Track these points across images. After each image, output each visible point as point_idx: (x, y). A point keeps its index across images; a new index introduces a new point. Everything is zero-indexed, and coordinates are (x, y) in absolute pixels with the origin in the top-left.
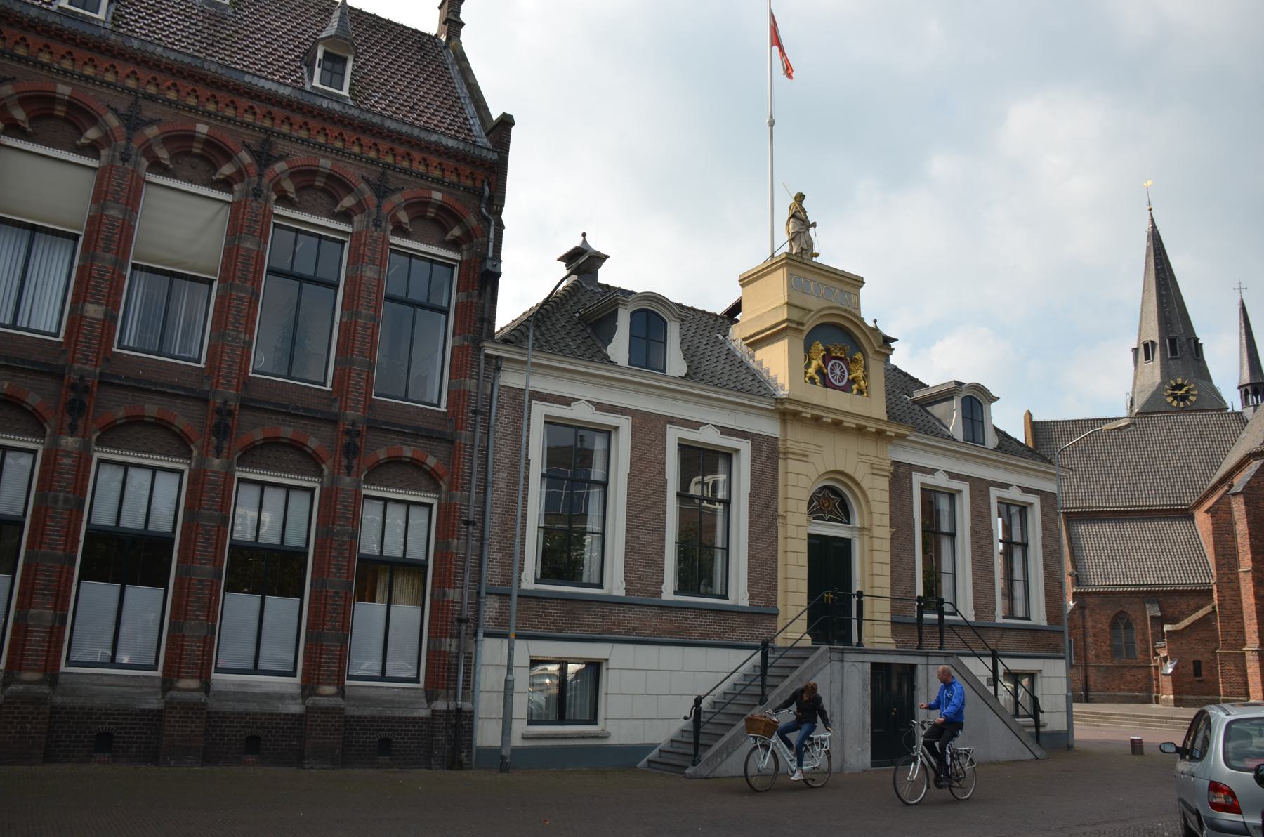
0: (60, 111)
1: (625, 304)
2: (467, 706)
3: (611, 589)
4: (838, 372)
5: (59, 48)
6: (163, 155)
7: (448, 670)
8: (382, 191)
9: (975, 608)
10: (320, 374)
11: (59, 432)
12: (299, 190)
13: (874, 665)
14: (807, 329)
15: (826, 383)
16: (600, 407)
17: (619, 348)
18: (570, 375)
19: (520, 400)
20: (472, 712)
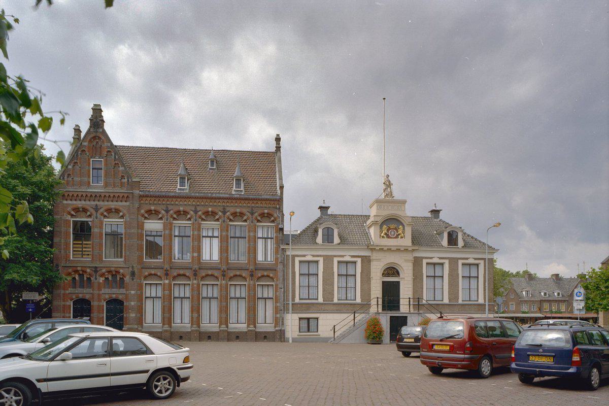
0: (266, 215)
2: (283, 329)
5: (179, 200)
6: (203, 217)
7: (279, 321)
8: (252, 214)
10: (243, 260)
11: (164, 280)
12: (234, 217)
14: (380, 223)
15: (388, 237)
16: (313, 256)
17: (319, 239)
20: (284, 330)
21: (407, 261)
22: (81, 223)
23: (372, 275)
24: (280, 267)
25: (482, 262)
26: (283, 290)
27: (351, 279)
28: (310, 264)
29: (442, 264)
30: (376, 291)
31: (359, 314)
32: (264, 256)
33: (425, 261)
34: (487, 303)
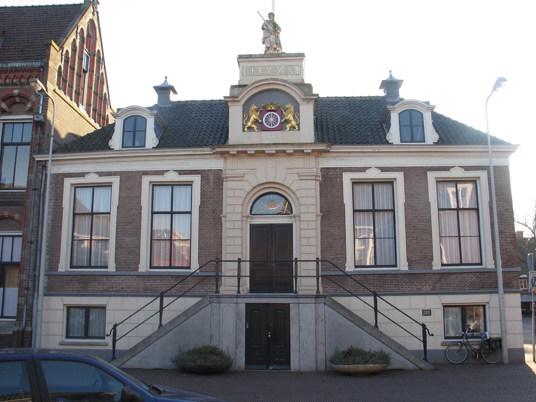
1: (394, 109)
2: (28, 329)
3: (486, 265)
4: (271, 120)
9: (408, 260)
13: (247, 304)
17: (394, 134)
18: (444, 154)
19: (59, 179)
21: (302, 177)
23: (227, 209)
24: (32, 199)
25: (483, 175)
26: (33, 246)
27: (383, 219)
28: (375, 186)
29: (391, 183)
30: (236, 246)
31: (172, 299)
33: (347, 178)
34: (500, 270)
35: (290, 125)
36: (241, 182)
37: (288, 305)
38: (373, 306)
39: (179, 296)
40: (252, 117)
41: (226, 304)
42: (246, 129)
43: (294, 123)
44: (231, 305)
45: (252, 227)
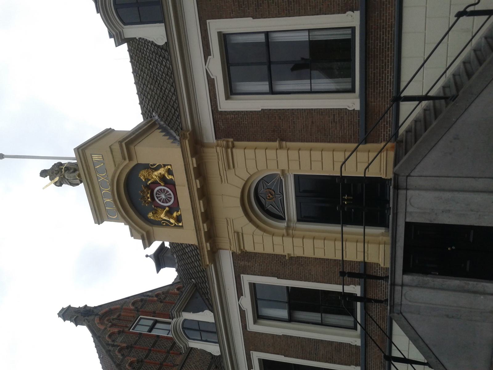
13: (406, 271)
15: (175, 207)
21: (230, 164)
22: (146, 246)
32: (223, 165)
35: (166, 175)
36: (244, 235)
37: (408, 225)
38: (417, 102)
39: (391, 342)
40: (164, 218)
41: (403, 297)
42: (180, 224)
43: (162, 171)
44: (404, 292)
45: (301, 218)
